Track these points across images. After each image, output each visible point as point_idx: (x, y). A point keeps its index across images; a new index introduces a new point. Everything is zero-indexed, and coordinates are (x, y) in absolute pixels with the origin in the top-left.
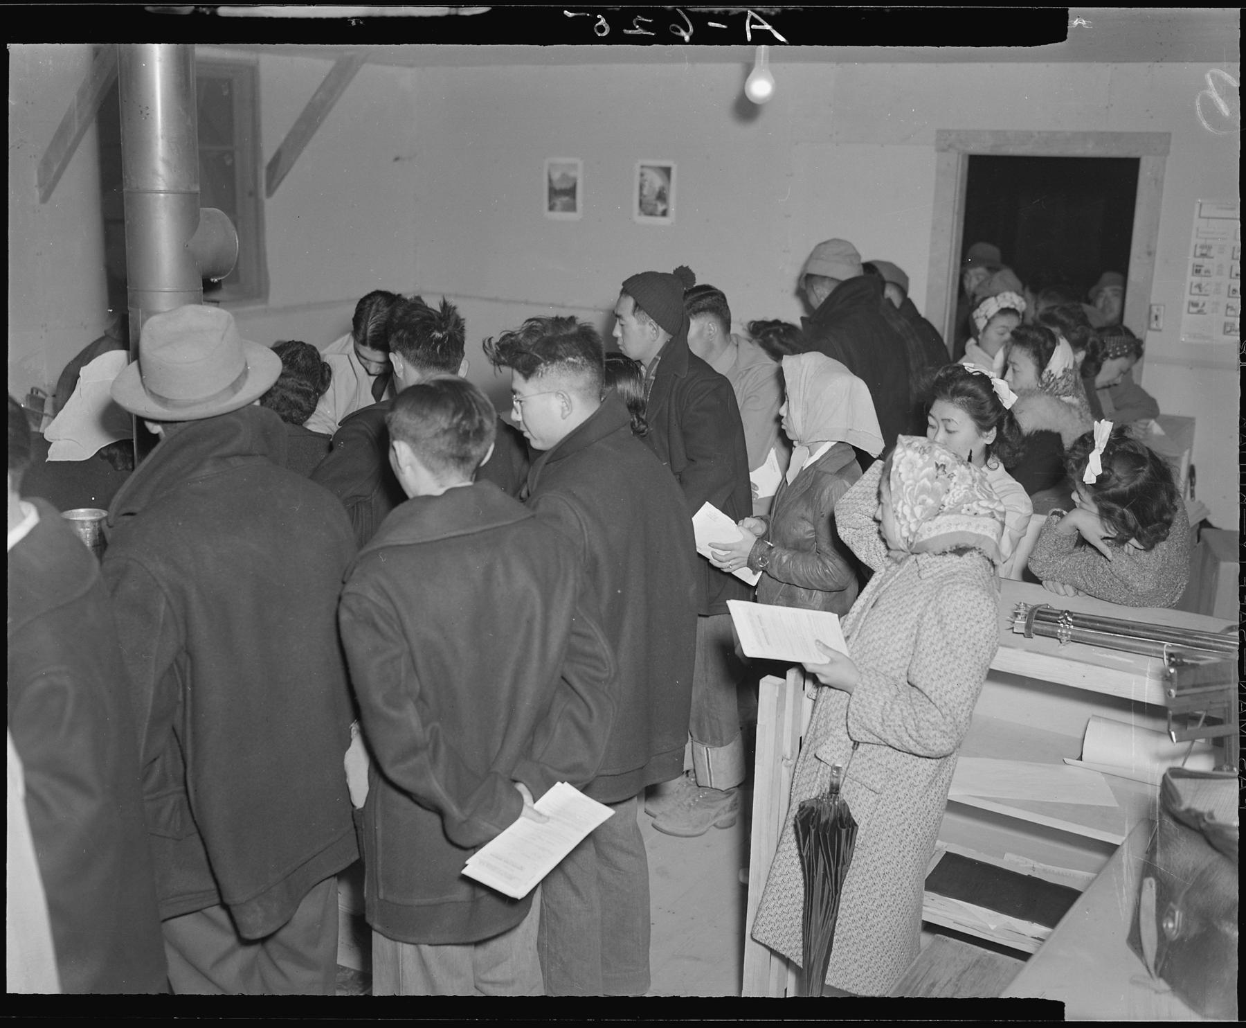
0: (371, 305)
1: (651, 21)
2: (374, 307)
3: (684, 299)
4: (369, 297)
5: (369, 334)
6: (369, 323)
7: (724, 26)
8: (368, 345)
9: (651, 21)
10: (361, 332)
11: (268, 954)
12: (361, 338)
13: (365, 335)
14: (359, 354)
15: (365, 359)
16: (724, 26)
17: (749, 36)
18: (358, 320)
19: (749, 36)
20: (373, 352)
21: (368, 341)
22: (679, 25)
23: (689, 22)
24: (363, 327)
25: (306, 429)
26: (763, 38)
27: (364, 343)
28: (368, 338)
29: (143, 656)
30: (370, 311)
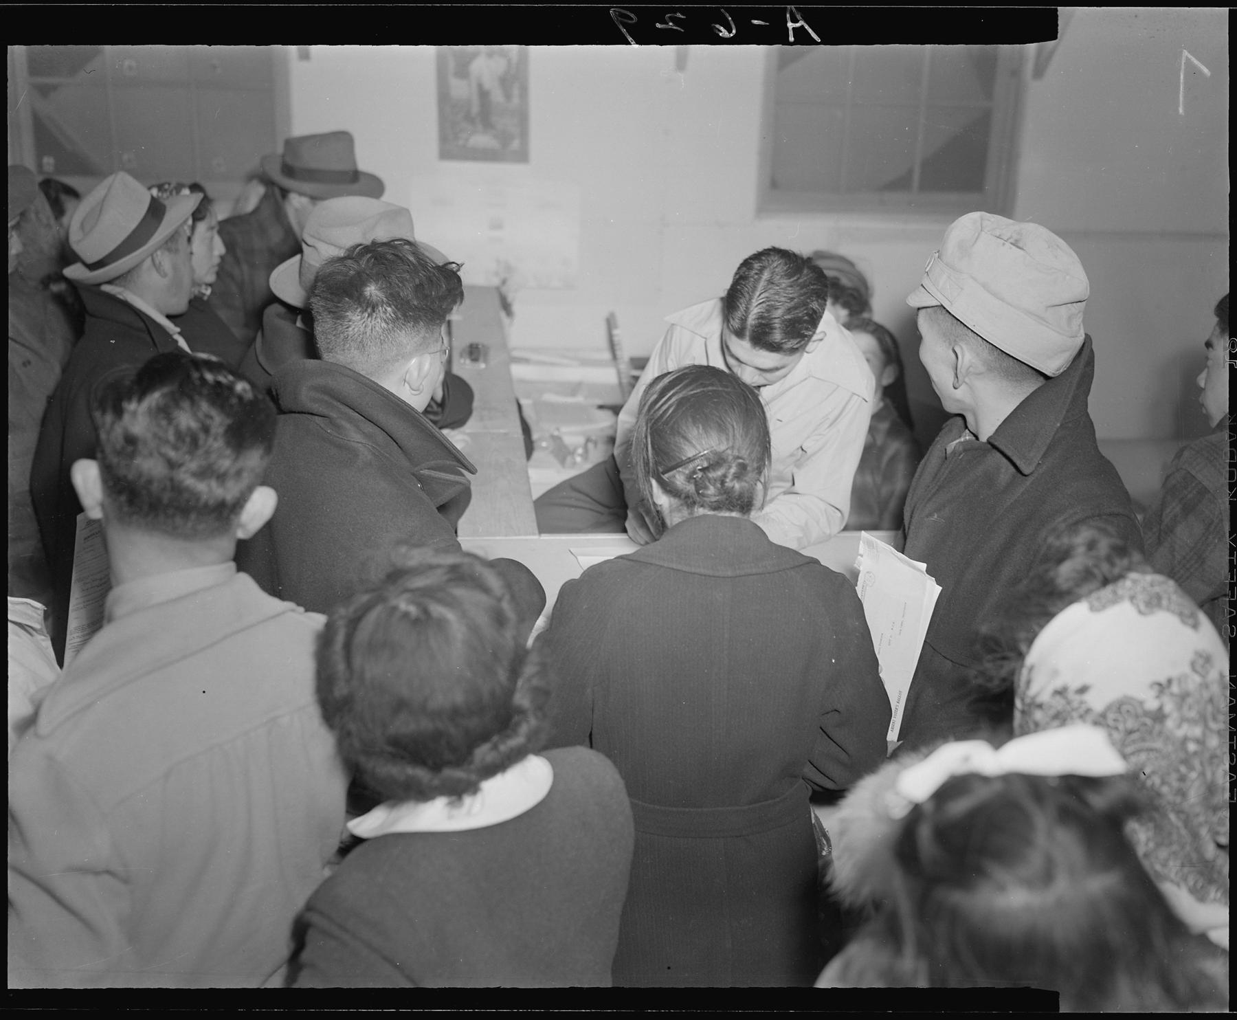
0: (761, 270)
1: (1181, 111)
2: (766, 275)
3: (55, 88)
4: (758, 256)
5: (751, 320)
6: (755, 302)
7: (682, 31)
8: (748, 338)
9: (1181, 111)
10: (739, 314)
11: (773, 399)
12: (736, 323)
13: (744, 320)
14: (728, 347)
15: (737, 359)
16: (682, 31)
17: (792, 39)
18: (731, 301)
19: (792, 39)
20: (754, 351)
21: (748, 333)
22: (735, 25)
23: (732, 23)
24: (742, 308)
25: (527, 472)
26: (802, 38)
27: (739, 333)
28: (749, 327)
29: (443, 307)
30: (757, 281)
